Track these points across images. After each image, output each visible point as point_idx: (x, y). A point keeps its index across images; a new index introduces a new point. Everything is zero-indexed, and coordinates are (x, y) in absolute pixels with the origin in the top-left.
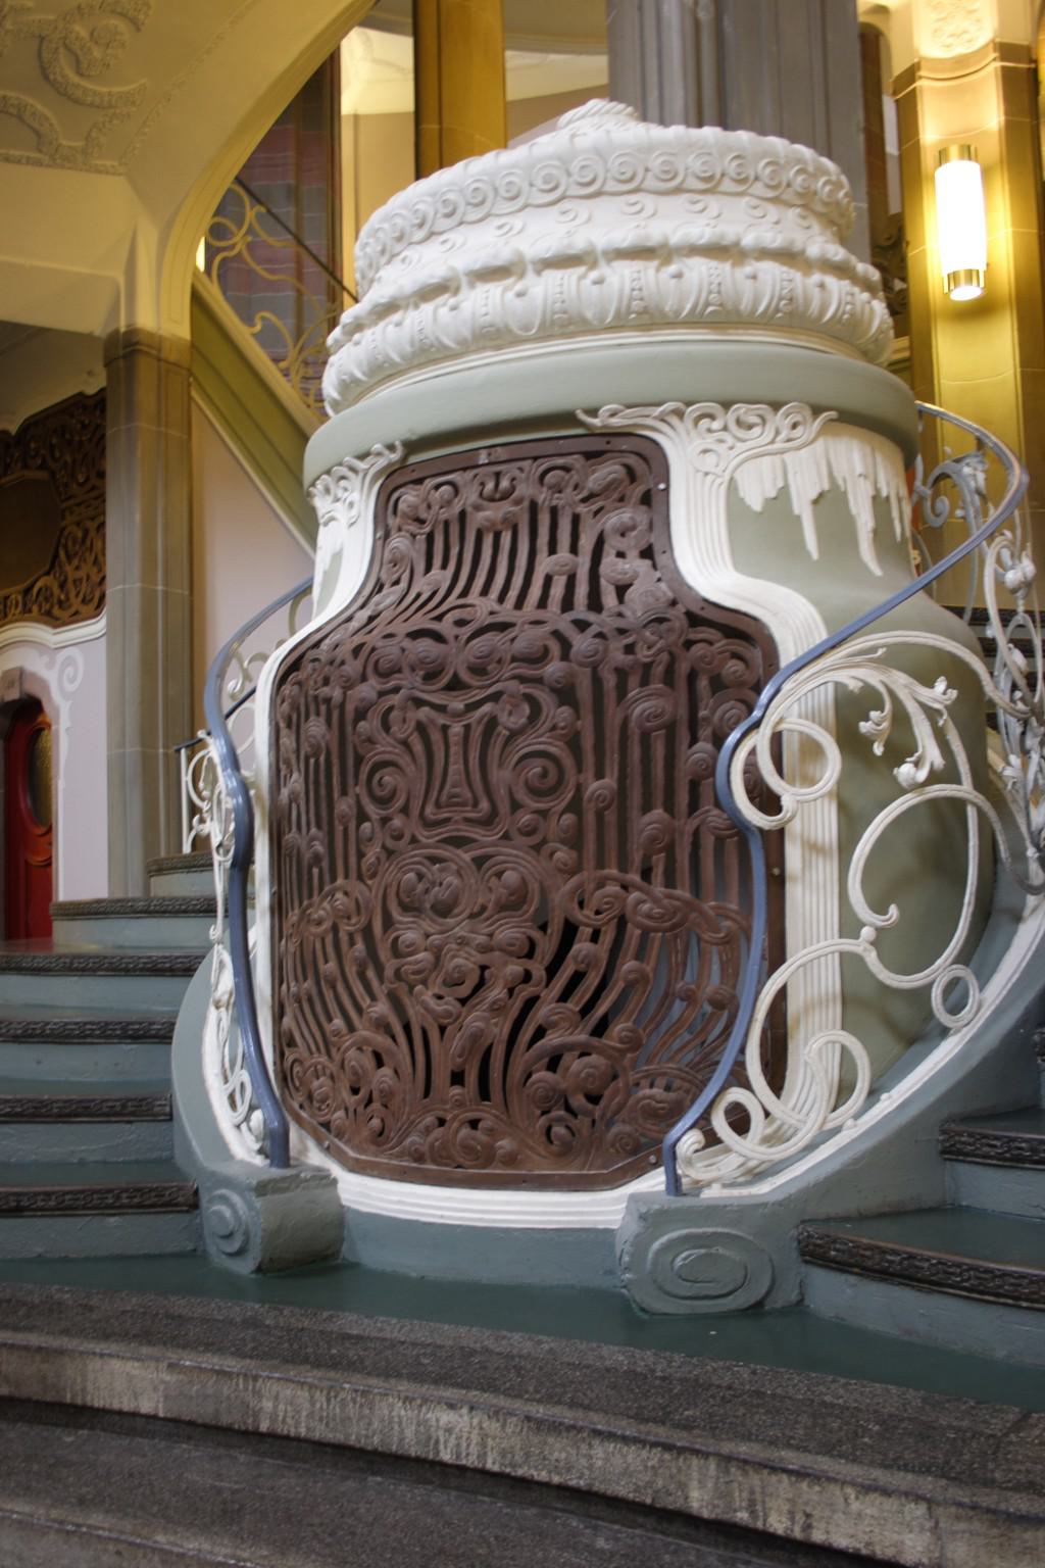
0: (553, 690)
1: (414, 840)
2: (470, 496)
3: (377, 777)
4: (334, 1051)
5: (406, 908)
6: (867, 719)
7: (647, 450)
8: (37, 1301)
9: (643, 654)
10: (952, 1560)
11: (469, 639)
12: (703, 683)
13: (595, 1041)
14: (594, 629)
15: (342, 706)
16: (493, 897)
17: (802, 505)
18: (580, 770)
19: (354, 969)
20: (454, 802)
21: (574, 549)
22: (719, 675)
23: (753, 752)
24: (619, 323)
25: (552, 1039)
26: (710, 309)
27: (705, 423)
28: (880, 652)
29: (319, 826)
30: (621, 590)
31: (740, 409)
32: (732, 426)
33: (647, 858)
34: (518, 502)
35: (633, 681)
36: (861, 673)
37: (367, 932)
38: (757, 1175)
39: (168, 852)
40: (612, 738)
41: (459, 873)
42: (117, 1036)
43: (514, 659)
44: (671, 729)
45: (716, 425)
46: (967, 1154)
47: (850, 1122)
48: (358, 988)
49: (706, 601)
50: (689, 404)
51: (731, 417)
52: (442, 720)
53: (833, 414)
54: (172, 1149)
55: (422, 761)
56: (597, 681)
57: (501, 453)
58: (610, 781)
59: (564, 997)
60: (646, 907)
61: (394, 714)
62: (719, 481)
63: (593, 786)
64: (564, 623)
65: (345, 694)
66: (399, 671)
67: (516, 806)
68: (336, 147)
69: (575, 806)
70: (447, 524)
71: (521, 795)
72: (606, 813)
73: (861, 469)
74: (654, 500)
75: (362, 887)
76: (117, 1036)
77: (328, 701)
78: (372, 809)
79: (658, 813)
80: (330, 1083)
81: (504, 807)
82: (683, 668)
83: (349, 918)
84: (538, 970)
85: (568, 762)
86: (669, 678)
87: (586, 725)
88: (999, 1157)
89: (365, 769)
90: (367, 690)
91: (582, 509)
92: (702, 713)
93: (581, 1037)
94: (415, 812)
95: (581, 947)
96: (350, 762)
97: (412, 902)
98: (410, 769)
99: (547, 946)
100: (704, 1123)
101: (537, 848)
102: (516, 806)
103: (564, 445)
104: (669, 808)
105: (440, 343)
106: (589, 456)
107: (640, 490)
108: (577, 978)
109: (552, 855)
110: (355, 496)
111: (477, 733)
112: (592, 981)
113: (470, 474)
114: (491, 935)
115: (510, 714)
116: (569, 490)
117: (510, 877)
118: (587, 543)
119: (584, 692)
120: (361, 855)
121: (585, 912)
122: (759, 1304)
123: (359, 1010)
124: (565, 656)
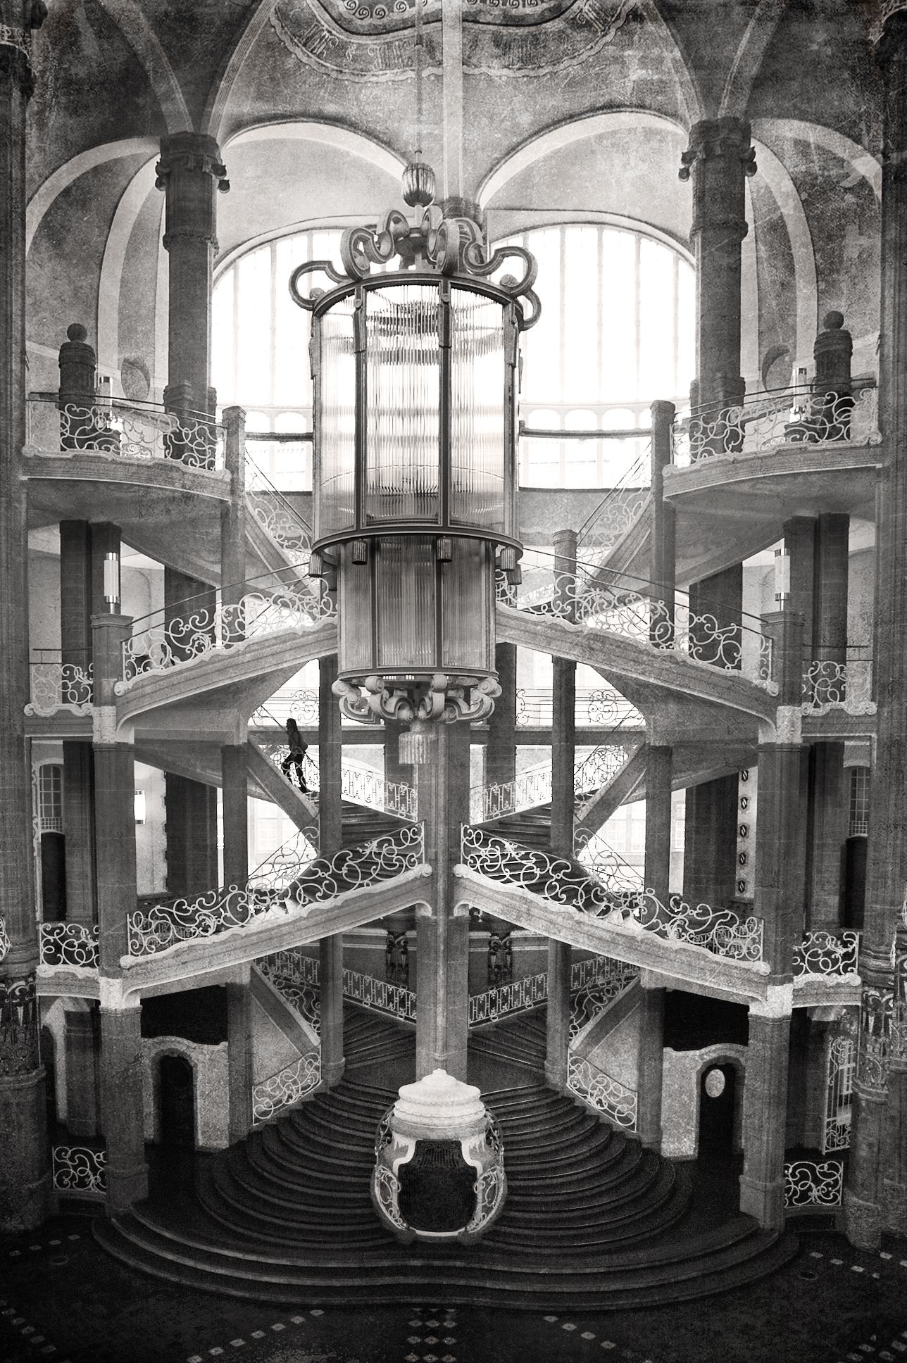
72: (160, 888)
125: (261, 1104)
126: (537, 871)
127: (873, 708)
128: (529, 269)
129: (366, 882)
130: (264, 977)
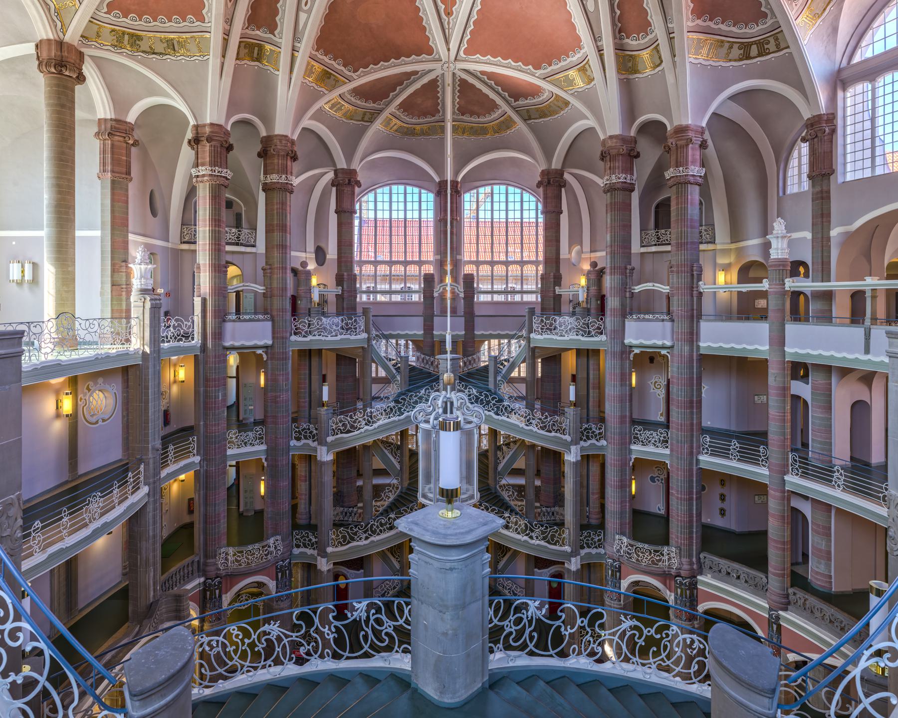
8: (260, 289)
10: (611, 137)
23: (587, 118)
39: (227, 252)
54: (58, 631)
68: (464, 447)
72: (703, 520)
73: (673, 572)
125: (82, 470)
127: (764, 280)
128: (600, 393)
129: (269, 662)
130: (307, 668)
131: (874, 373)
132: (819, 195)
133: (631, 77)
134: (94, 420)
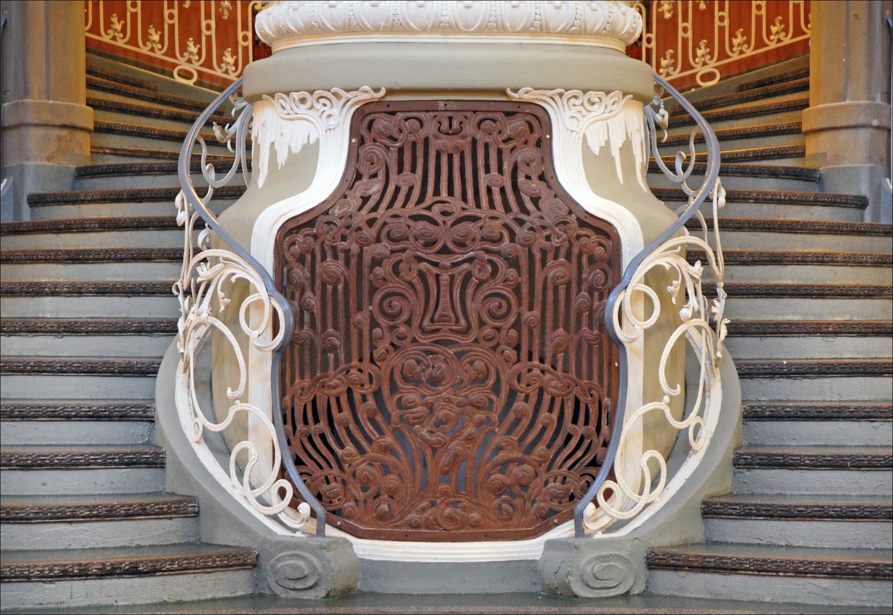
0: (506, 259)
1: (414, 340)
2: (430, 128)
3: (387, 301)
4: (346, 466)
5: (406, 379)
6: (671, 285)
7: (540, 113)
9: (555, 242)
11: (453, 225)
12: (585, 259)
13: (526, 457)
14: (528, 225)
15: (360, 256)
16: (467, 375)
17: (616, 153)
18: (520, 305)
19: (365, 416)
20: (444, 319)
21: (500, 171)
22: (592, 255)
24: (525, 31)
25: (502, 456)
26: (573, 28)
27: (573, 101)
28: (680, 248)
29: (335, 327)
30: (535, 200)
31: (593, 95)
32: (586, 104)
33: (554, 357)
34: (464, 137)
35: (550, 256)
36: (669, 259)
37: (377, 395)
38: (618, 525)
40: (538, 288)
41: (446, 361)
42: (115, 464)
43: (482, 239)
44: (568, 284)
45: (578, 102)
46: (719, 514)
47: (658, 499)
48: (369, 427)
49: (587, 212)
50: (566, 90)
51: (586, 97)
52: (435, 270)
53: (631, 96)
55: (422, 295)
56: (531, 256)
57: (455, 106)
58: (536, 312)
59: (509, 432)
60: (554, 383)
61: (402, 265)
62: (579, 136)
63: (526, 314)
64: (509, 219)
65: (361, 249)
66: (407, 239)
67: (482, 324)
69: (517, 325)
70: (414, 144)
71: (486, 319)
74: (543, 144)
75: (374, 367)
76: (115, 464)
77: (347, 252)
78: (381, 320)
79: (561, 330)
80: (341, 486)
81: (474, 324)
82: (575, 250)
83: (362, 385)
84: (495, 417)
85: (513, 301)
86: (568, 257)
87: (524, 279)
88: (738, 514)
89: (378, 297)
90: (384, 247)
91: (502, 146)
92: (584, 276)
93: (517, 454)
94: (416, 322)
95: (519, 404)
96: (366, 291)
97: (413, 377)
98: (413, 299)
99: (499, 402)
100: (595, 502)
101: (494, 348)
102: (482, 324)
103: (495, 107)
104: (567, 329)
105: (407, 23)
106: (508, 114)
107: (536, 136)
108: (518, 421)
109: (503, 352)
110: (335, 111)
111: (458, 282)
112: (525, 422)
113: (432, 114)
114: (466, 397)
115: (480, 270)
116: (495, 134)
117: (479, 364)
118: (507, 167)
119: (524, 262)
120: (373, 347)
121: (522, 385)
122: (628, 592)
123: (370, 441)
124: (512, 240)
126: (402, 329)
131: (152, 421)
132: (500, 26)
133: (25, 163)
134: (322, 101)
